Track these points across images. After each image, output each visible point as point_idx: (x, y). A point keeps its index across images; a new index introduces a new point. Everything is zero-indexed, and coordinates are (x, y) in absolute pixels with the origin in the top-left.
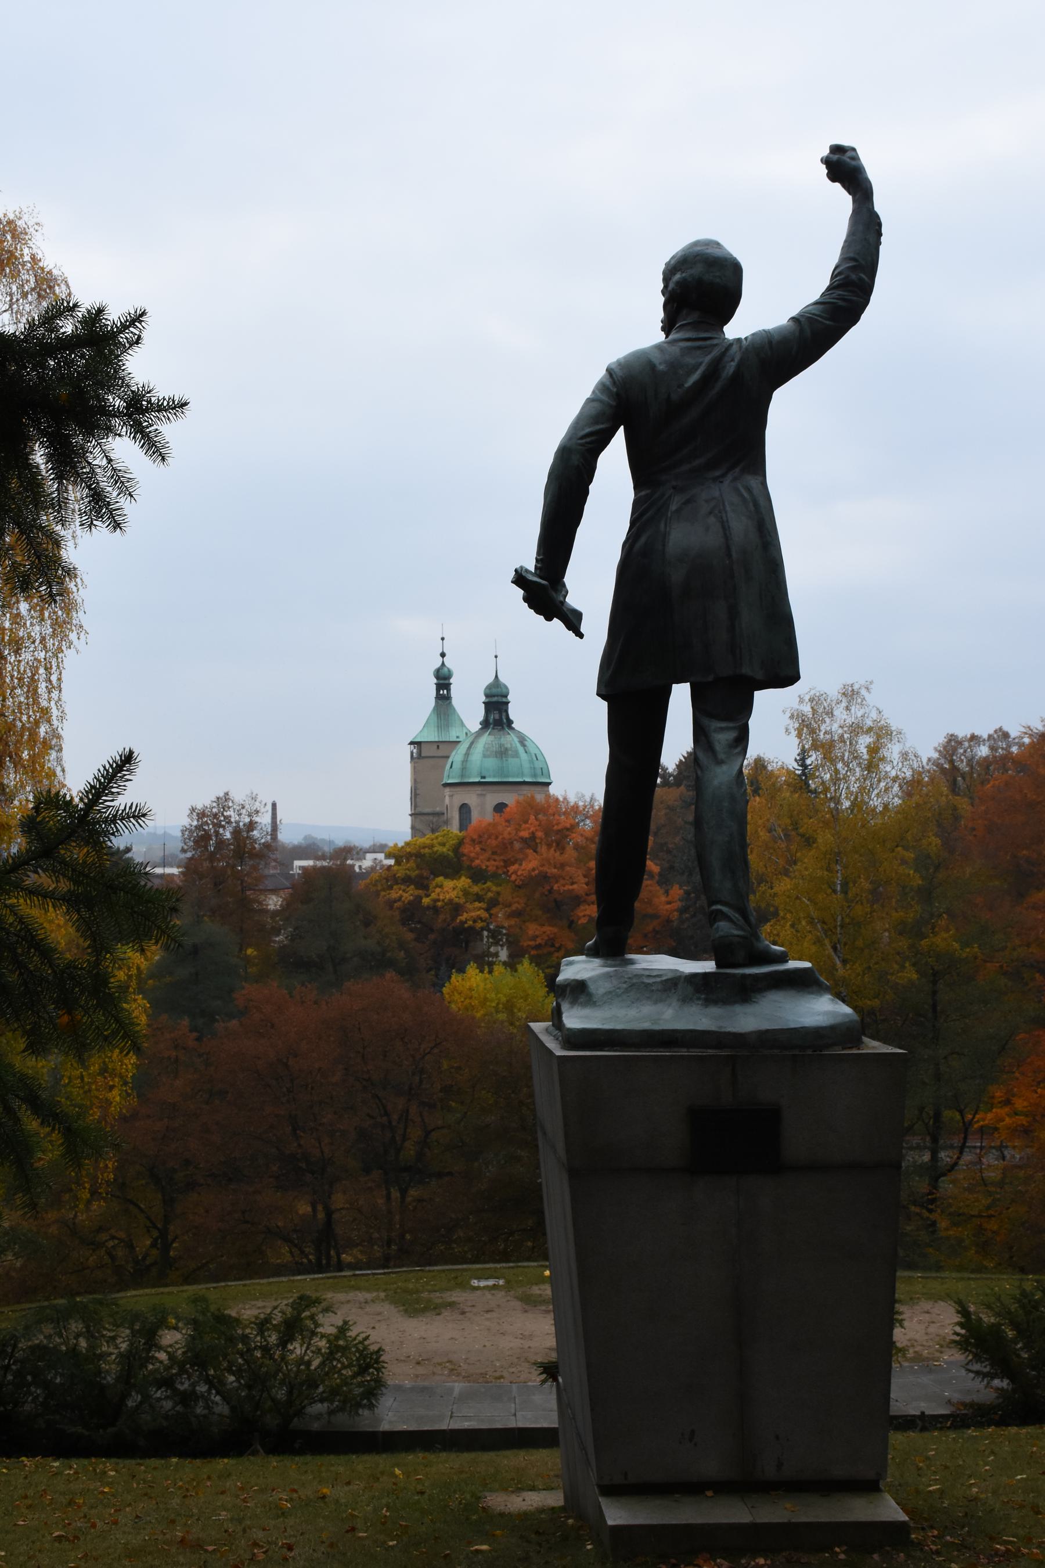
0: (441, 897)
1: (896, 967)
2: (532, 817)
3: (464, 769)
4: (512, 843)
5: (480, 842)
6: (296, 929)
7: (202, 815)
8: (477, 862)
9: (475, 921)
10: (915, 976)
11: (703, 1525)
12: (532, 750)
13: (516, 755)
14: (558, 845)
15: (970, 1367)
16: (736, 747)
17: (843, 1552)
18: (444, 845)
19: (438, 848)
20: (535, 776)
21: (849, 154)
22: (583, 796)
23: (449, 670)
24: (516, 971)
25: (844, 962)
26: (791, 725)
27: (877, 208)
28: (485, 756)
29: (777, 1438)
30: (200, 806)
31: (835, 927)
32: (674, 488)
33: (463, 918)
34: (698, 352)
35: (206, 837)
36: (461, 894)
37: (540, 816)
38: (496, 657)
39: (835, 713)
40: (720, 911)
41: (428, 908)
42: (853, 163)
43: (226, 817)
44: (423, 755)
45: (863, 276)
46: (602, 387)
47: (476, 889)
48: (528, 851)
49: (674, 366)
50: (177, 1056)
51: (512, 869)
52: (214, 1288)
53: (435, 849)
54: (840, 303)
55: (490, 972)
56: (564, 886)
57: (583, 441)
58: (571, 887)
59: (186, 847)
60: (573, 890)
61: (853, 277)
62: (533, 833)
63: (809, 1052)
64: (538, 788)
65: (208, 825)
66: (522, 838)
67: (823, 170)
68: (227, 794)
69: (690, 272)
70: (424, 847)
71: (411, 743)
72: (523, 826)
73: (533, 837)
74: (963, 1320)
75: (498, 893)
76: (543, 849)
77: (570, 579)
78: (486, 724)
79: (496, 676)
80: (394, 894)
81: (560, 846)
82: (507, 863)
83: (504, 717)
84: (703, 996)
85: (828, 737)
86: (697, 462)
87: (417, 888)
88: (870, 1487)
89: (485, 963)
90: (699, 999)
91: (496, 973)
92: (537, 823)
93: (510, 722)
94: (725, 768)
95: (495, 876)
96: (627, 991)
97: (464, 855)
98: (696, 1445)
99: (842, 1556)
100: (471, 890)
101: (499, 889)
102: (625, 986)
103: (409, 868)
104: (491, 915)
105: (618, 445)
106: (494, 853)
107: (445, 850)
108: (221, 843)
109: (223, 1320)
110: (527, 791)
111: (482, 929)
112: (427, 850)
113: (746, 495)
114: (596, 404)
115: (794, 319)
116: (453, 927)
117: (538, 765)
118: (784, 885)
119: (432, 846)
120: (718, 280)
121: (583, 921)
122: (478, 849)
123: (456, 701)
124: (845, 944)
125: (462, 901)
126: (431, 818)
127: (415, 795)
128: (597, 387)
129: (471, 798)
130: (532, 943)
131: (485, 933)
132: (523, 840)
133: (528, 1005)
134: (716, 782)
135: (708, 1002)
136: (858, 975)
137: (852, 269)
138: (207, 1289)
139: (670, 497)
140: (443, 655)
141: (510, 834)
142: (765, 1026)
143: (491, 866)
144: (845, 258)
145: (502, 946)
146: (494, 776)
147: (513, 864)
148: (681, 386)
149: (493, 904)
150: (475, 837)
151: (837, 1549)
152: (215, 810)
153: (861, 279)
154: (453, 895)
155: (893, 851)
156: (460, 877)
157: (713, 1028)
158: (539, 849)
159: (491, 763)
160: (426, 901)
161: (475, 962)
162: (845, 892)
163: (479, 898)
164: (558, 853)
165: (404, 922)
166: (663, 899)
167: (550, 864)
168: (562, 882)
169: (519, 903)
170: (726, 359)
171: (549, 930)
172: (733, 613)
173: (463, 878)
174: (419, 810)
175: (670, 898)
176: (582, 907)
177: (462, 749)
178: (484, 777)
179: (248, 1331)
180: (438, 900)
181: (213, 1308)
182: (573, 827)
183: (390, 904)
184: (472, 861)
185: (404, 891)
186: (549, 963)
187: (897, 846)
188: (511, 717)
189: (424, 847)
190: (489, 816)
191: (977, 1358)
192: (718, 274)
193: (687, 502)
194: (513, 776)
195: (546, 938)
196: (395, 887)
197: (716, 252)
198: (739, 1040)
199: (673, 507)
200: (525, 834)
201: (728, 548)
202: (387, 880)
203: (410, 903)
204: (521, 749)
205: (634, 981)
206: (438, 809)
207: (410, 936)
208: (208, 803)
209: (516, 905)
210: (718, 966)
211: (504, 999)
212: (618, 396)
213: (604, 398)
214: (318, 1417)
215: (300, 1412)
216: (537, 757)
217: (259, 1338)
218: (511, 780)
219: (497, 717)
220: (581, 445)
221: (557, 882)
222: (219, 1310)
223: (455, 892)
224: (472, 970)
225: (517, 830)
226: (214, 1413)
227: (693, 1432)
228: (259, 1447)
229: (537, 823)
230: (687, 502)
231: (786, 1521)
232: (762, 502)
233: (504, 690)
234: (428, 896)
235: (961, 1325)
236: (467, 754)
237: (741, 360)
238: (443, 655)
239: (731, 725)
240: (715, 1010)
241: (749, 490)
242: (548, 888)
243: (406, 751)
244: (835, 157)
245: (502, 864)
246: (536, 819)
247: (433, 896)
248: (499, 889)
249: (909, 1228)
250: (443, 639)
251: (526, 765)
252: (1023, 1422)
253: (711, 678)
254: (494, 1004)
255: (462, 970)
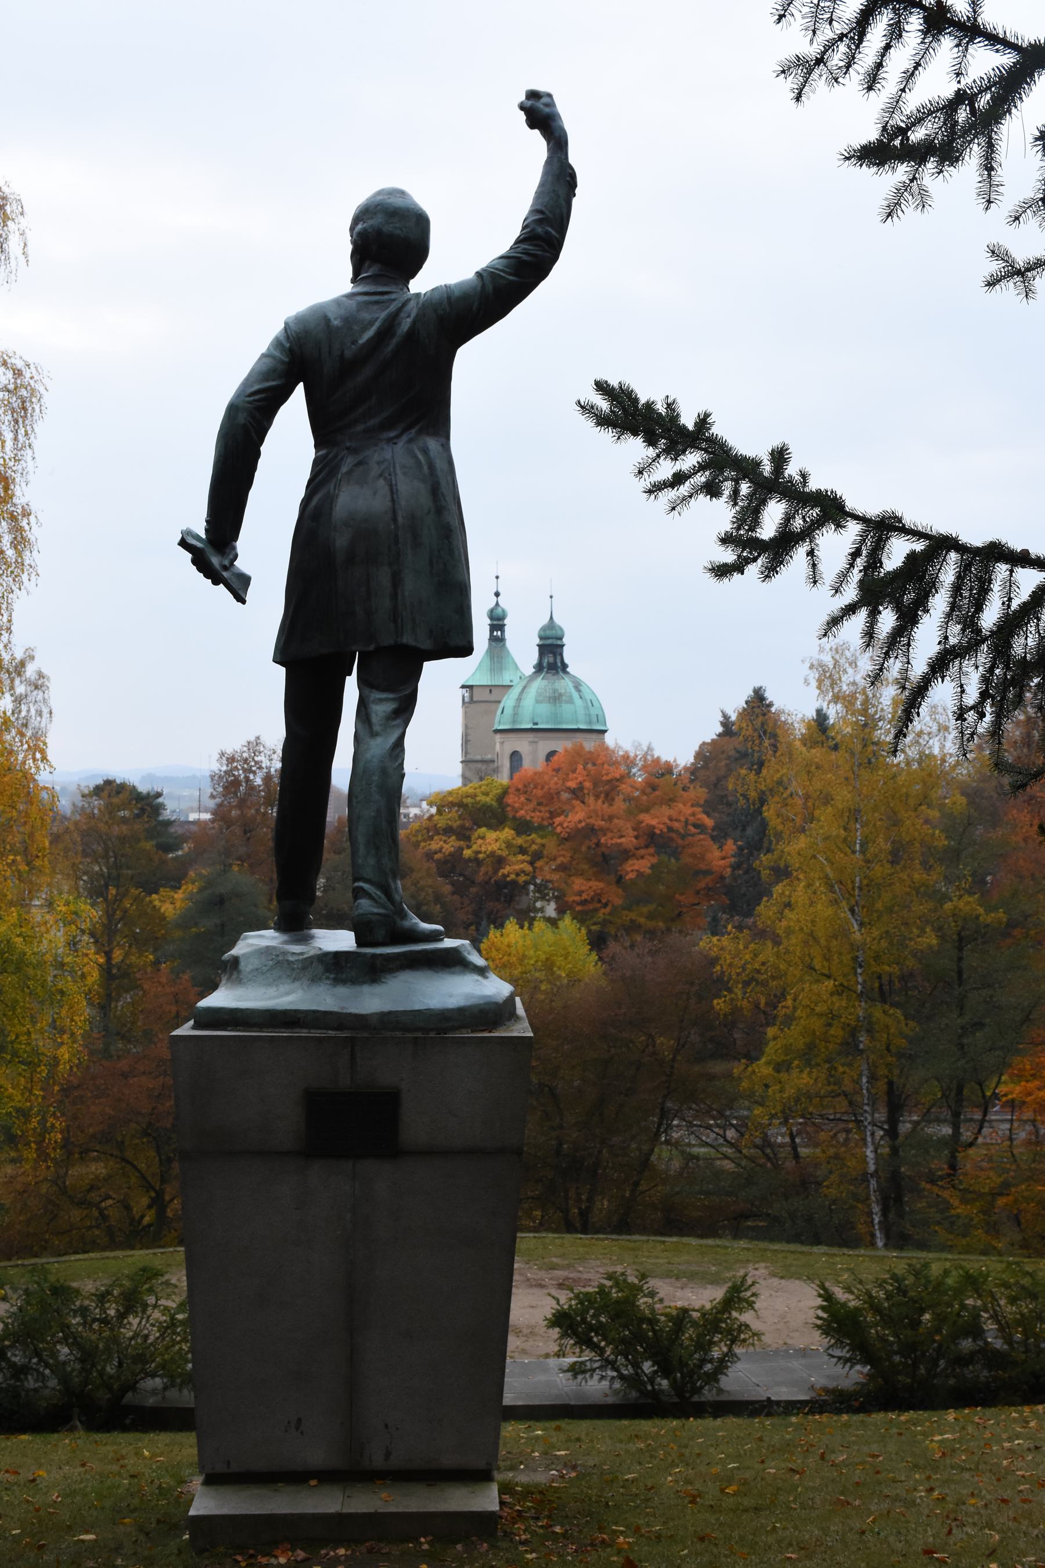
0: (483, 849)
1: (916, 931)
2: (580, 767)
3: (515, 714)
4: (558, 793)
5: (526, 792)
6: (328, 879)
7: (231, 760)
8: (522, 812)
9: (518, 875)
10: (934, 942)
11: (286, 1515)
12: (588, 696)
13: (571, 701)
14: (607, 795)
15: (830, 1351)
16: (394, 719)
17: (427, 1542)
18: (487, 794)
19: (482, 798)
20: (590, 723)
21: (544, 100)
22: (640, 745)
23: (503, 611)
24: (557, 928)
25: (861, 924)
26: (812, 675)
27: (572, 160)
28: (537, 701)
29: (386, 1426)
30: (229, 751)
31: (853, 889)
32: (348, 448)
33: (505, 871)
34: (375, 307)
35: (236, 783)
36: (504, 845)
37: (589, 766)
38: (551, 597)
39: (859, 664)
40: (362, 888)
41: (469, 860)
42: (547, 110)
43: (256, 763)
44: (475, 699)
45: (550, 229)
46: (277, 343)
47: (520, 841)
48: (574, 802)
49: (349, 321)
50: (178, 1012)
51: (558, 820)
52: (162, 1253)
53: (478, 799)
54: (525, 258)
55: (530, 928)
56: (612, 839)
57: (251, 398)
58: (619, 841)
59: (215, 793)
60: (621, 844)
61: (539, 230)
62: (581, 783)
63: (432, 1035)
64: (594, 736)
65: (238, 770)
66: (569, 788)
67: (522, 116)
68: (258, 738)
69: (371, 222)
70: (467, 796)
71: (463, 687)
72: (571, 776)
73: (581, 788)
74: (825, 1303)
75: (543, 846)
76: (591, 800)
77: (242, 544)
78: (539, 668)
79: (551, 618)
80: (434, 845)
81: (609, 797)
82: (553, 815)
83: (558, 661)
84: (332, 976)
85: (852, 688)
86: (373, 422)
87: (459, 839)
88: (482, 1476)
89: (526, 918)
90: (328, 978)
91: (536, 929)
92: (585, 773)
93: (564, 666)
94: (379, 740)
95: (541, 828)
96: (272, 968)
97: (509, 805)
98: (302, 1433)
99: (426, 1547)
100: (514, 842)
101: (543, 841)
102: (271, 963)
103: (452, 817)
104: (535, 868)
105: (297, 401)
106: (540, 804)
107: (488, 799)
108: (251, 788)
109: (62, 1292)
110: (579, 738)
111: (527, 883)
112: (469, 800)
113: (420, 457)
114: (267, 360)
115: (479, 274)
116: (495, 881)
117: (594, 712)
118: (802, 842)
119: (475, 796)
120: (398, 232)
121: (632, 876)
122: (522, 799)
123: (509, 644)
124: (863, 907)
125: (505, 853)
126: (480, 765)
127: (466, 741)
128: (272, 344)
129: (522, 744)
130: (577, 898)
131: (532, 887)
132: (573, 791)
133: (569, 963)
134: (368, 756)
135: (338, 981)
136: (874, 939)
137: (539, 222)
138: (154, 1254)
139: (343, 458)
140: (497, 594)
141: (556, 784)
142: (387, 1007)
143: (536, 818)
144: (534, 211)
145: (548, 901)
146: (547, 723)
147: (559, 815)
148: (354, 342)
149: (537, 856)
150: (520, 786)
151: (423, 1540)
152: (245, 755)
153: (547, 233)
154: (495, 847)
155: (916, 810)
156: (503, 829)
157: (336, 1009)
158: (586, 800)
159: (544, 709)
160: (467, 853)
161: (514, 917)
162: (863, 852)
163: (522, 850)
164: (606, 805)
165: (443, 874)
166: (717, 853)
167: (598, 816)
168: (609, 835)
169: (564, 856)
170: (402, 315)
171: (597, 885)
172: (396, 581)
173: (507, 830)
174: (470, 757)
175: (724, 854)
176: (630, 862)
177: (514, 693)
178: (536, 724)
179: (87, 1302)
180: (480, 852)
181: (52, 1279)
182: (621, 779)
183: (429, 856)
184: (517, 812)
185: (445, 842)
186: (595, 920)
187: (920, 805)
188: (566, 661)
189: (467, 796)
190: (540, 764)
191: (839, 1344)
192: (398, 225)
193: (359, 464)
194: (567, 723)
195: (592, 893)
196: (436, 838)
197: (398, 202)
198: (360, 1021)
199: (344, 469)
200: (572, 784)
201: (394, 512)
202: (428, 830)
203: (451, 854)
204: (575, 695)
205: (280, 958)
206: (489, 757)
207: (447, 889)
208: (238, 747)
209: (562, 859)
210: (360, 942)
211: (543, 957)
212: (291, 352)
213: (277, 354)
214: (154, 1392)
215: (132, 1387)
216: (591, 703)
217: (97, 1311)
218: (564, 727)
219: (551, 660)
220: (249, 402)
221: (605, 835)
222: (58, 1281)
223: (498, 844)
224: (511, 926)
225: (564, 780)
226: (47, 1387)
227: (299, 1420)
228: (78, 1423)
229: (585, 773)
230: (359, 464)
231: (372, 1511)
232: (440, 464)
233: (559, 632)
234: (469, 847)
235: (822, 1308)
236: (519, 699)
237: (417, 316)
238: (497, 594)
239: (391, 696)
240: (342, 990)
241: (425, 451)
242: (595, 840)
243: (458, 695)
244: (529, 103)
245: (548, 815)
246: (585, 768)
247: (475, 847)
248: (543, 841)
249: (919, 1205)
250: (497, 577)
251: (581, 713)
252: (885, 1407)
253: (372, 647)
254: (532, 962)
255: (500, 926)
